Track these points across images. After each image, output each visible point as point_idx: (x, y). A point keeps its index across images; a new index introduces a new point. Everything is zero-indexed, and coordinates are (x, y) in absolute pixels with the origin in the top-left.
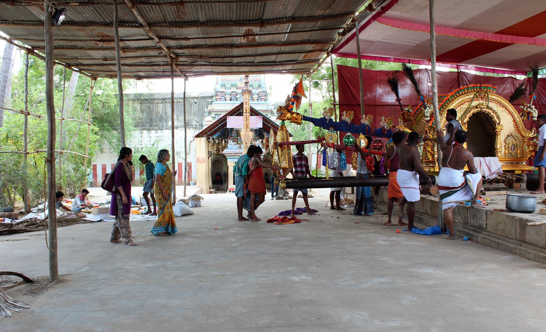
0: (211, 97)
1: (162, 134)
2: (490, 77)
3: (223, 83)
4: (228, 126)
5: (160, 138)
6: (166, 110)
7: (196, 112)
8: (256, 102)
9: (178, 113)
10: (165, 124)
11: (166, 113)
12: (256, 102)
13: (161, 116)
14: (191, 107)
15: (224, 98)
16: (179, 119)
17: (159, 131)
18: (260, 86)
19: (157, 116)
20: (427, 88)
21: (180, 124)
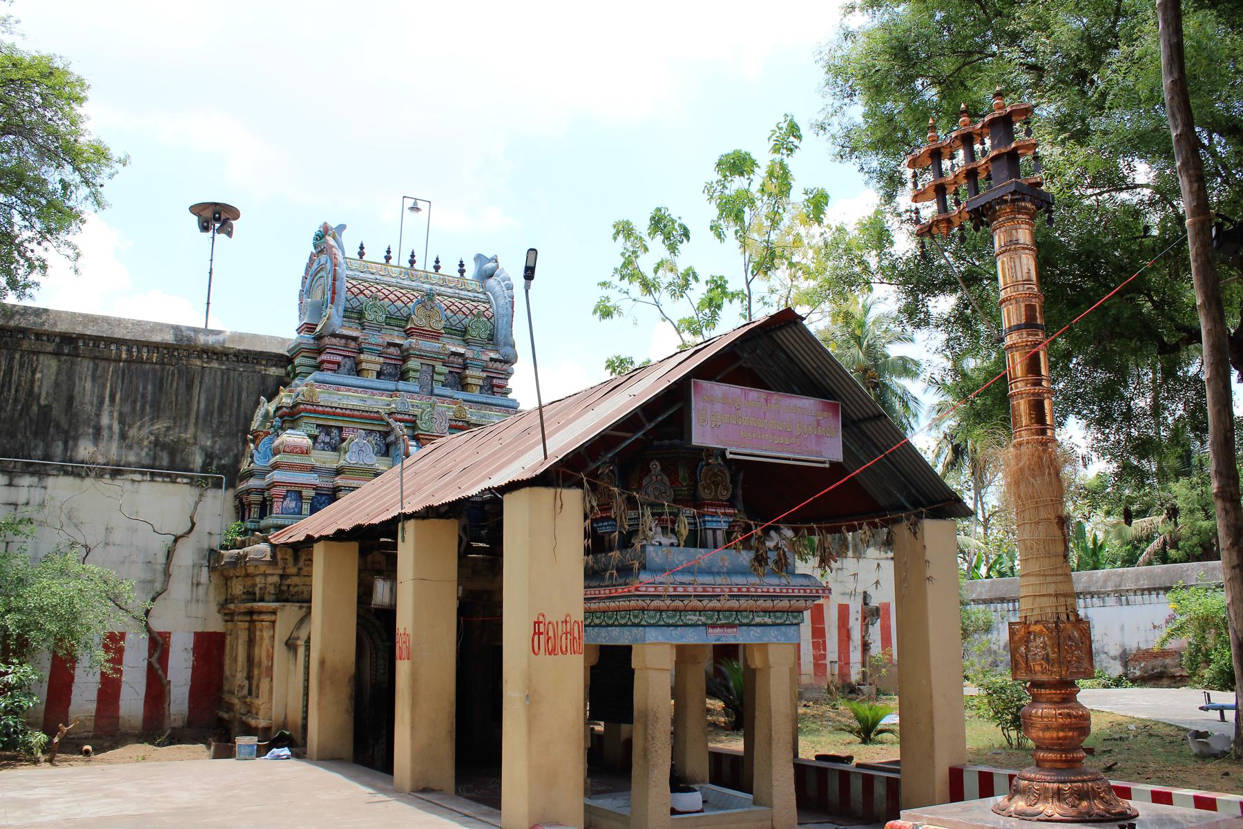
0: (284, 361)
1: (37, 495)
2: (658, 416)
3: (355, 303)
4: (701, 436)
5: (25, 512)
6: (71, 388)
7: (209, 412)
8: (475, 395)
9: (127, 409)
10: (58, 448)
11: (71, 399)
12: (475, 395)
13: (45, 411)
14: (189, 387)
15: (349, 363)
16: (133, 432)
17: (26, 480)
18: (492, 338)
19: (26, 408)
20: (1032, 580)
21: (132, 458)
